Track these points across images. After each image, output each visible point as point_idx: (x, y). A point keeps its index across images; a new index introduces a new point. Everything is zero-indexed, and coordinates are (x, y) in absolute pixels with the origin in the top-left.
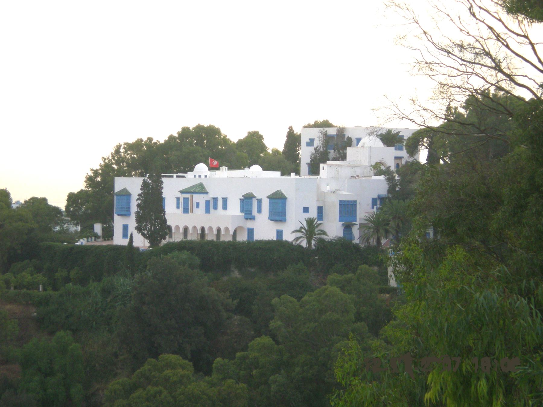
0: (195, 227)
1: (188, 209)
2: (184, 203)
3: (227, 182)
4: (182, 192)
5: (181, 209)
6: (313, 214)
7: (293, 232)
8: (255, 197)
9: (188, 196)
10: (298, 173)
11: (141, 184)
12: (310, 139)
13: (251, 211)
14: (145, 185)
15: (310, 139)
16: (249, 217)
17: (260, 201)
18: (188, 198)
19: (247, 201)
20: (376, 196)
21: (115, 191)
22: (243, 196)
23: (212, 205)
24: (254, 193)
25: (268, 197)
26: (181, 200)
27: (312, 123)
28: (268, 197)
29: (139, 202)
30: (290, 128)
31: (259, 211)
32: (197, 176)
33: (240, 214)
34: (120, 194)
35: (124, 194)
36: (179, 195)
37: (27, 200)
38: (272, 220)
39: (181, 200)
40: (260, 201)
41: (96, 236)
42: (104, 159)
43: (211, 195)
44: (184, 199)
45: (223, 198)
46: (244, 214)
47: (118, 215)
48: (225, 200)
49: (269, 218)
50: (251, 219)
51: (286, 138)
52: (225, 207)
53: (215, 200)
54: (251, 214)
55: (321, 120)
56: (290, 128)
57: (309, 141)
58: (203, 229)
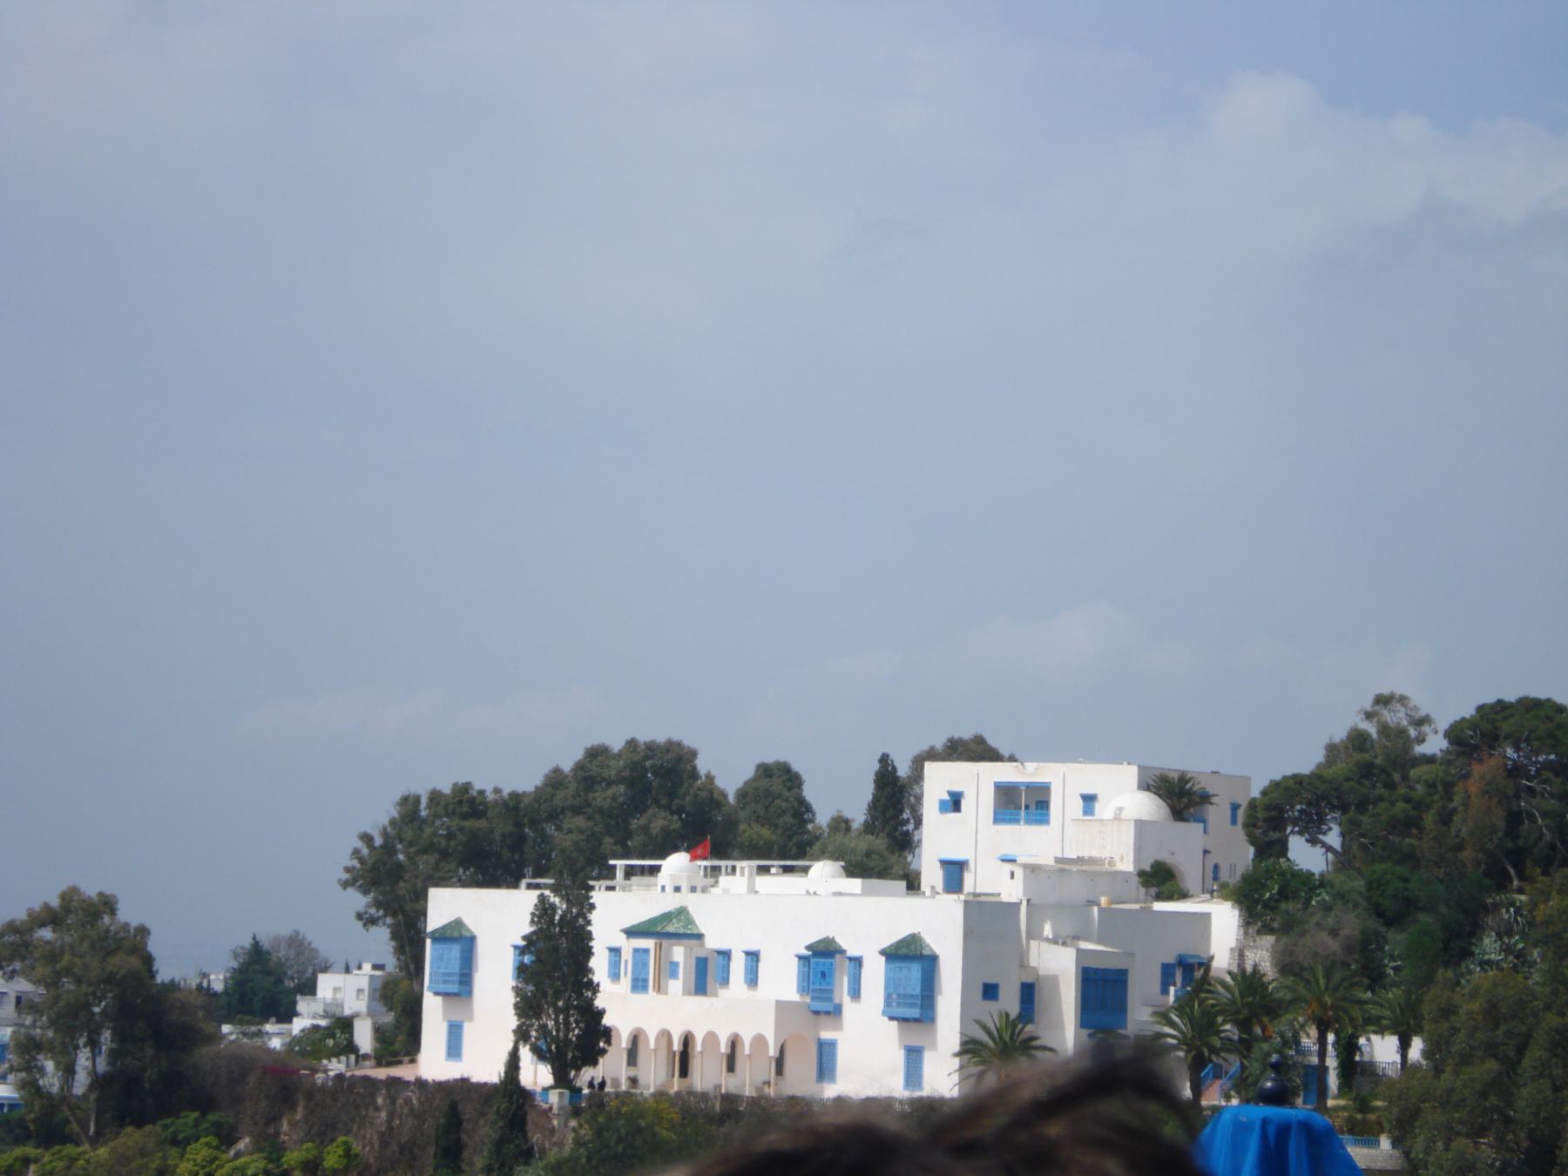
0: (666, 1035)
1: (646, 981)
2: (635, 965)
3: (764, 912)
4: (631, 932)
5: (626, 981)
6: (1010, 1002)
7: (978, 1022)
8: (843, 952)
9: (649, 944)
10: (913, 885)
11: (531, 909)
12: (950, 793)
13: (831, 991)
14: (544, 911)
15: (950, 793)
16: (822, 1006)
17: (857, 962)
18: (646, 951)
19: (823, 958)
20: (1171, 960)
21: (429, 929)
22: (808, 948)
23: (707, 975)
24: (838, 940)
25: (883, 952)
26: (627, 955)
27: (939, 743)
28: (883, 952)
29: (527, 959)
30: (884, 759)
31: (856, 994)
32: (669, 889)
33: (796, 997)
34: (442, 936)
35: (456, 934)
36: (621, 941)
37: (528, 929)
38: (892, 1018)
39: (627, 955)
40: (857, 962)
41: (361, 1058)
42: (367, 838)
43: (712, 943)
44: (636, 951)
45: (748, 953)
46: (808, 1000)
47: (437, 994)
48: (753, 956)
49: (884, 1013)
50: (828, 1013)
51: (872, 786)
52: (752, 980)
53: (726, 955)
54: (830, 999)
55: (966, 734)
56: (884, 759)
57: (947, 797)
58: (687, 1040)
